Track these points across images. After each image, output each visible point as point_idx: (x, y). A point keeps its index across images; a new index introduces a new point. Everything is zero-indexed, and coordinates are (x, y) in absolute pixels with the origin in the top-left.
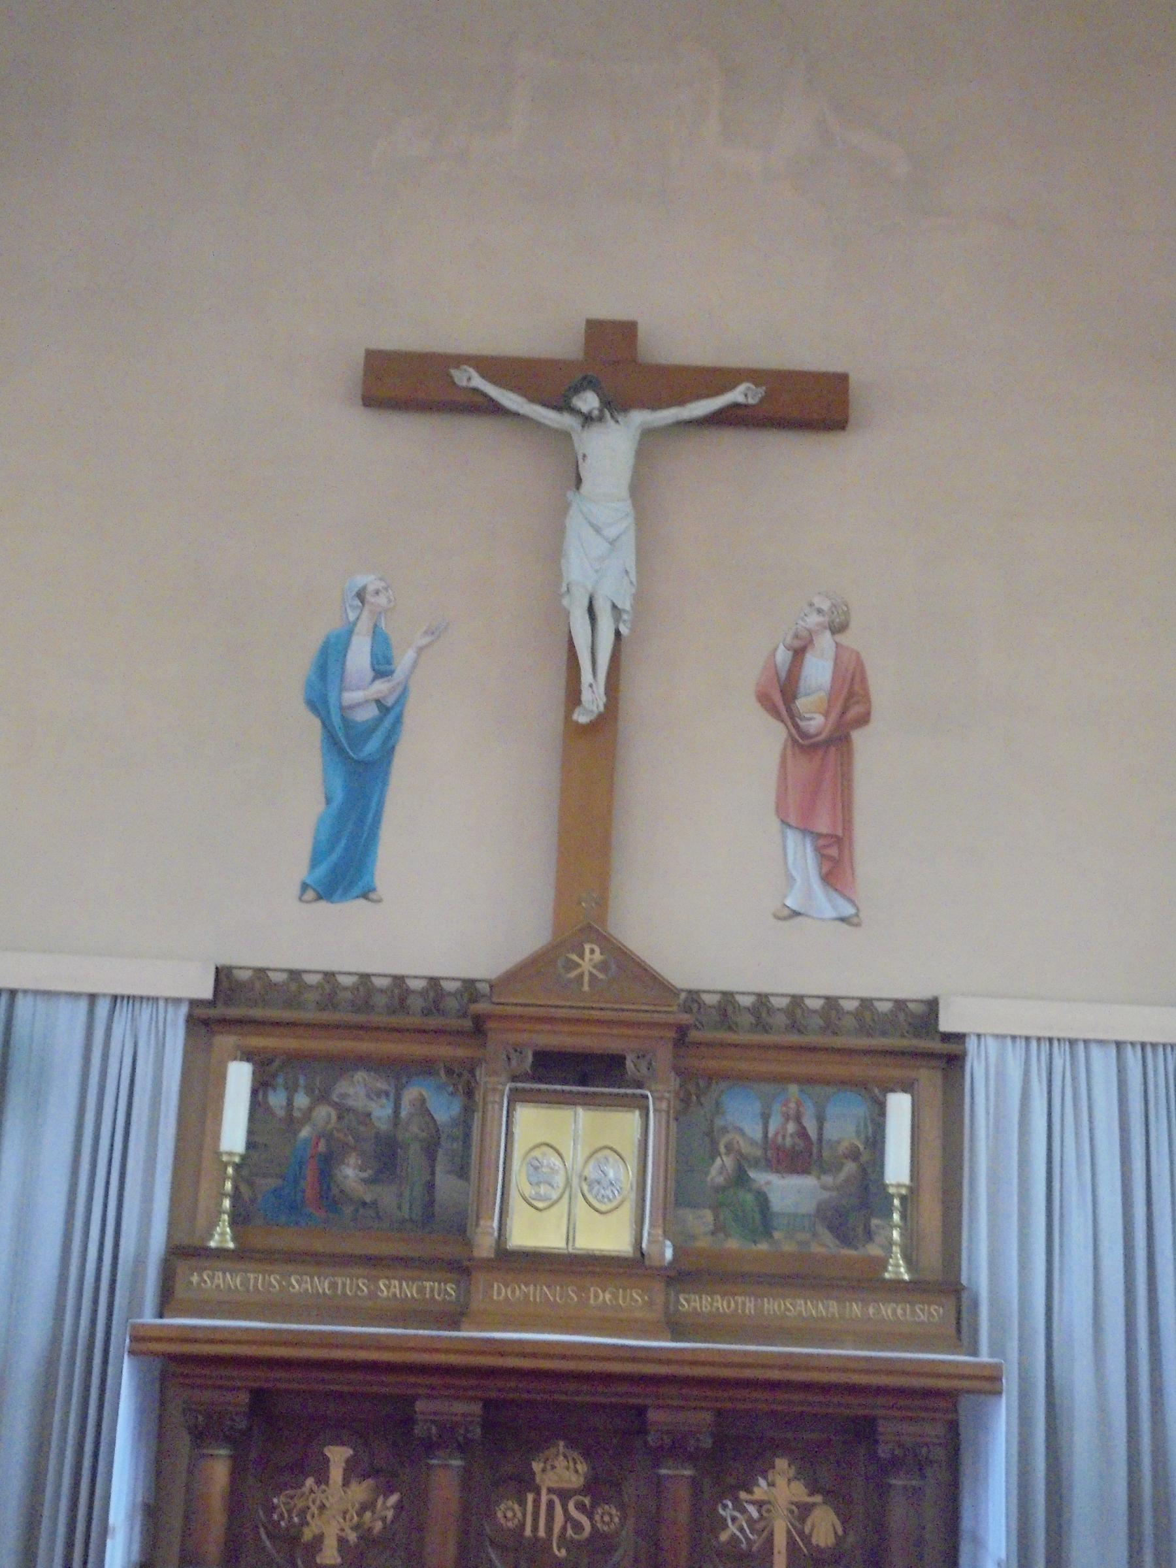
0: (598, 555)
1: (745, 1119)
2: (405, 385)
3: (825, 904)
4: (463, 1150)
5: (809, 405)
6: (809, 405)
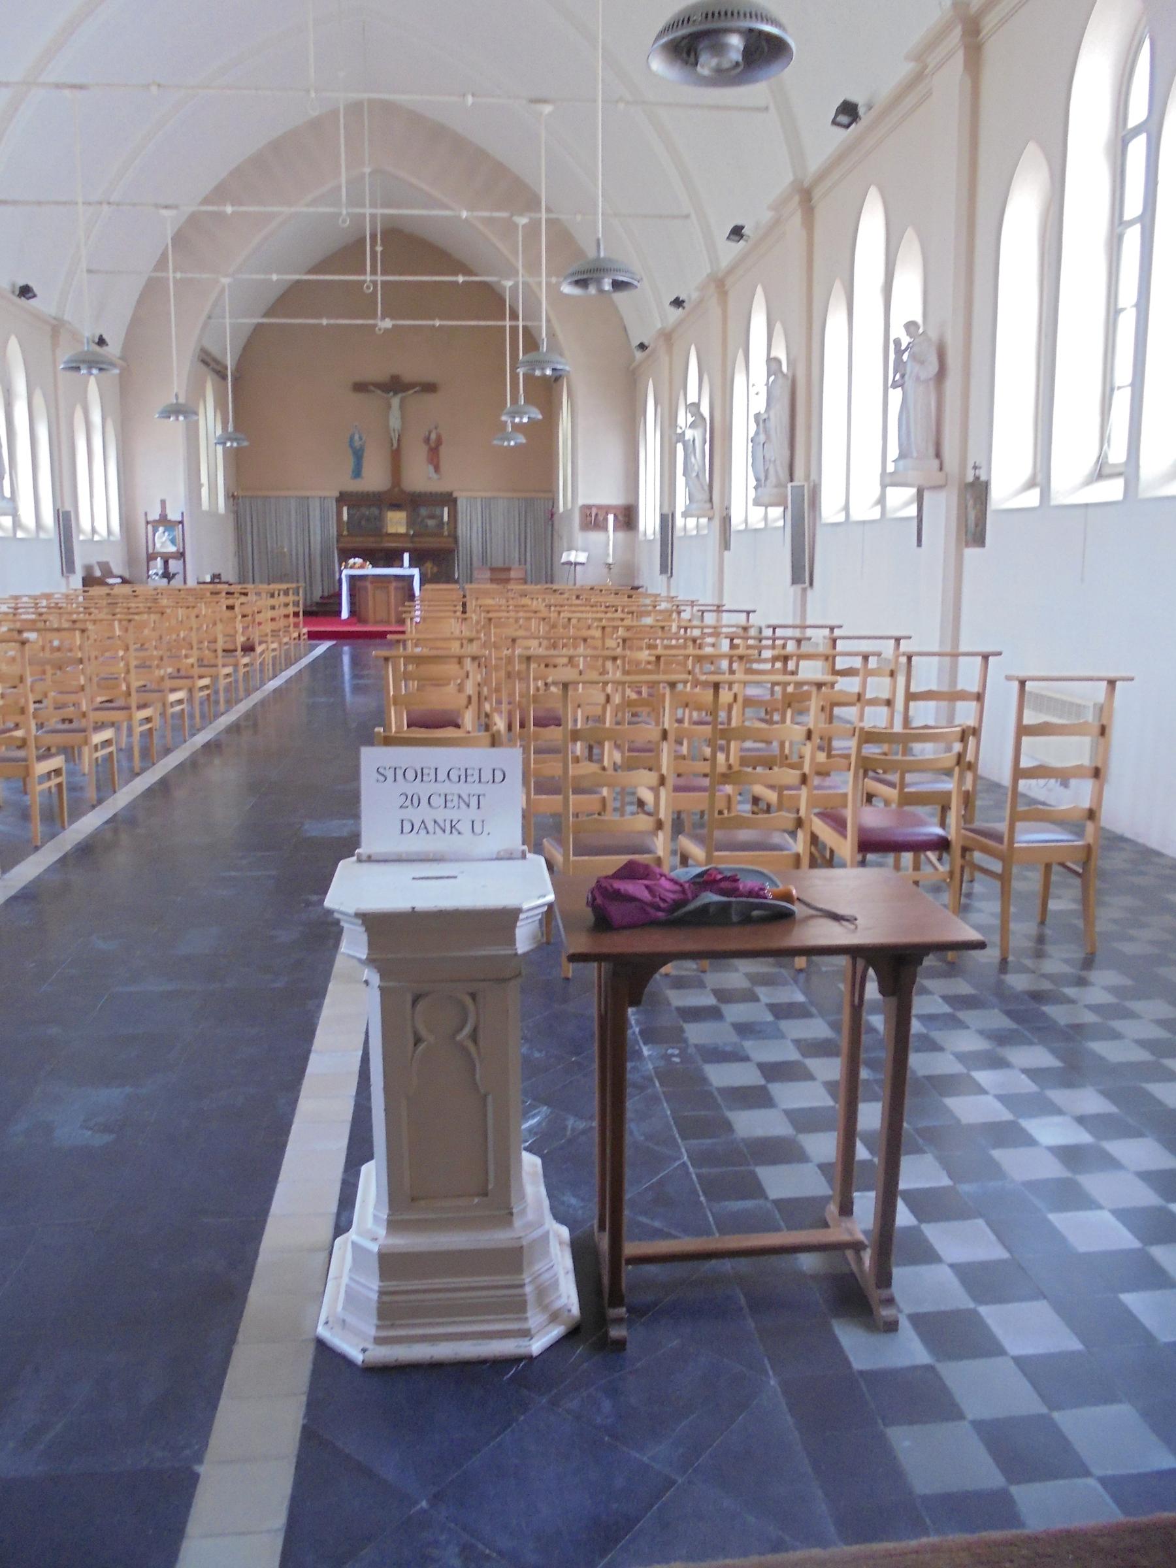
0: (395, 422)
1: (423, 511)
2: (360, 387)
3: (435, 476)
4: (380, 519)
5: (430, 388)
6: (430, 388)
